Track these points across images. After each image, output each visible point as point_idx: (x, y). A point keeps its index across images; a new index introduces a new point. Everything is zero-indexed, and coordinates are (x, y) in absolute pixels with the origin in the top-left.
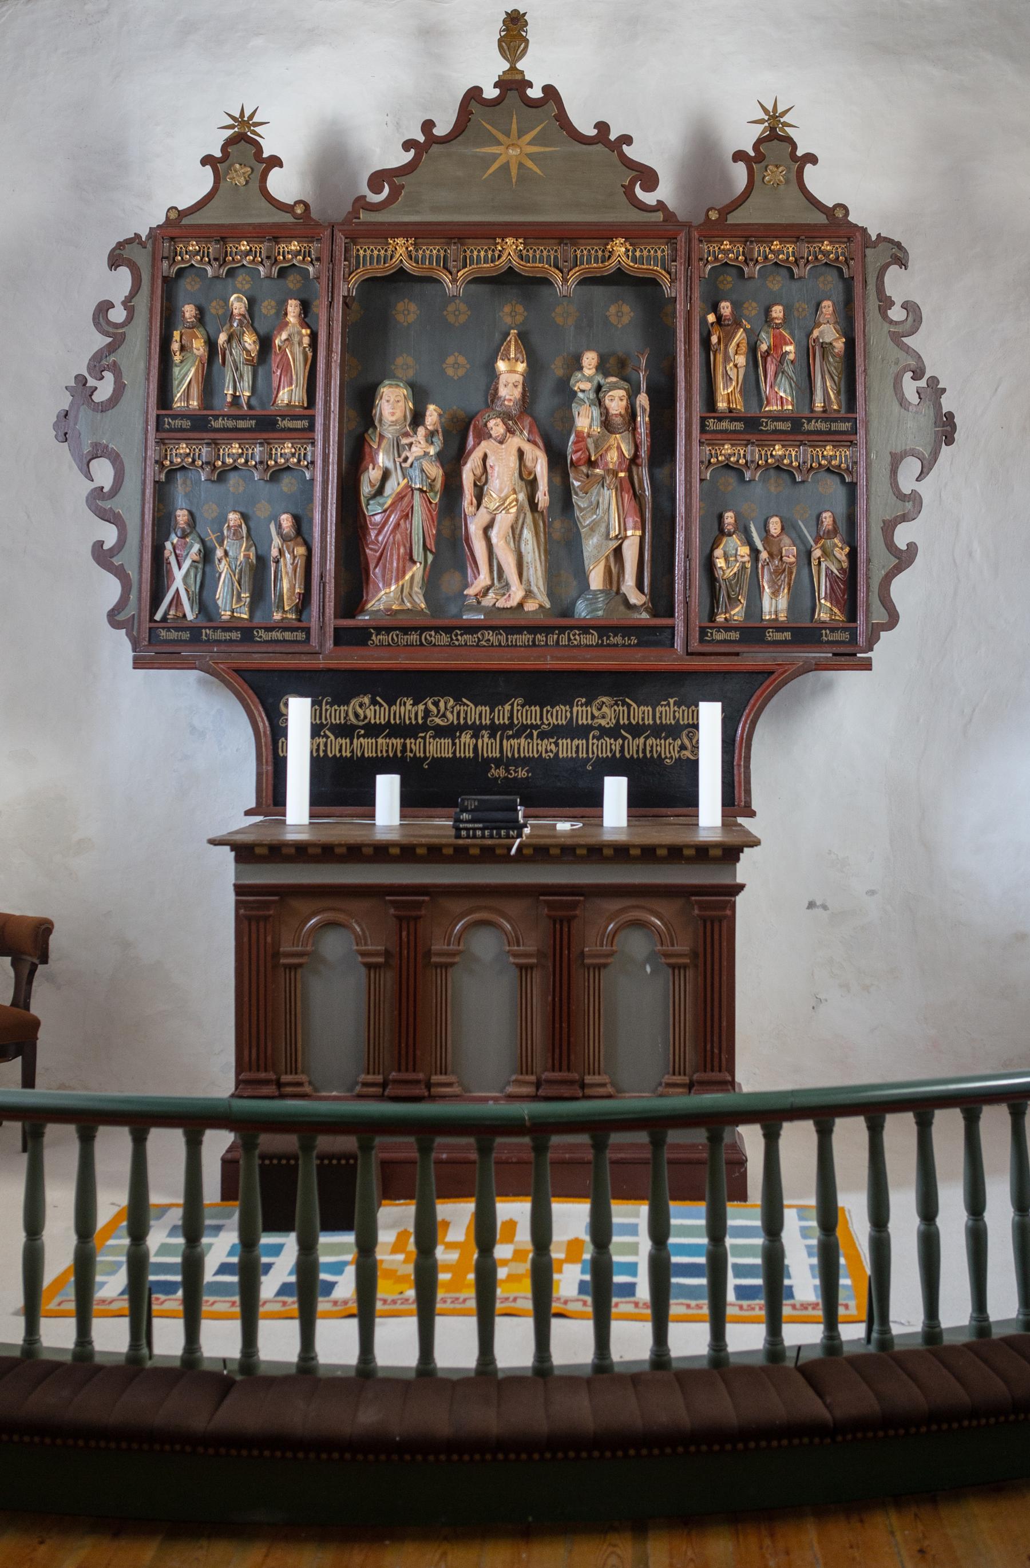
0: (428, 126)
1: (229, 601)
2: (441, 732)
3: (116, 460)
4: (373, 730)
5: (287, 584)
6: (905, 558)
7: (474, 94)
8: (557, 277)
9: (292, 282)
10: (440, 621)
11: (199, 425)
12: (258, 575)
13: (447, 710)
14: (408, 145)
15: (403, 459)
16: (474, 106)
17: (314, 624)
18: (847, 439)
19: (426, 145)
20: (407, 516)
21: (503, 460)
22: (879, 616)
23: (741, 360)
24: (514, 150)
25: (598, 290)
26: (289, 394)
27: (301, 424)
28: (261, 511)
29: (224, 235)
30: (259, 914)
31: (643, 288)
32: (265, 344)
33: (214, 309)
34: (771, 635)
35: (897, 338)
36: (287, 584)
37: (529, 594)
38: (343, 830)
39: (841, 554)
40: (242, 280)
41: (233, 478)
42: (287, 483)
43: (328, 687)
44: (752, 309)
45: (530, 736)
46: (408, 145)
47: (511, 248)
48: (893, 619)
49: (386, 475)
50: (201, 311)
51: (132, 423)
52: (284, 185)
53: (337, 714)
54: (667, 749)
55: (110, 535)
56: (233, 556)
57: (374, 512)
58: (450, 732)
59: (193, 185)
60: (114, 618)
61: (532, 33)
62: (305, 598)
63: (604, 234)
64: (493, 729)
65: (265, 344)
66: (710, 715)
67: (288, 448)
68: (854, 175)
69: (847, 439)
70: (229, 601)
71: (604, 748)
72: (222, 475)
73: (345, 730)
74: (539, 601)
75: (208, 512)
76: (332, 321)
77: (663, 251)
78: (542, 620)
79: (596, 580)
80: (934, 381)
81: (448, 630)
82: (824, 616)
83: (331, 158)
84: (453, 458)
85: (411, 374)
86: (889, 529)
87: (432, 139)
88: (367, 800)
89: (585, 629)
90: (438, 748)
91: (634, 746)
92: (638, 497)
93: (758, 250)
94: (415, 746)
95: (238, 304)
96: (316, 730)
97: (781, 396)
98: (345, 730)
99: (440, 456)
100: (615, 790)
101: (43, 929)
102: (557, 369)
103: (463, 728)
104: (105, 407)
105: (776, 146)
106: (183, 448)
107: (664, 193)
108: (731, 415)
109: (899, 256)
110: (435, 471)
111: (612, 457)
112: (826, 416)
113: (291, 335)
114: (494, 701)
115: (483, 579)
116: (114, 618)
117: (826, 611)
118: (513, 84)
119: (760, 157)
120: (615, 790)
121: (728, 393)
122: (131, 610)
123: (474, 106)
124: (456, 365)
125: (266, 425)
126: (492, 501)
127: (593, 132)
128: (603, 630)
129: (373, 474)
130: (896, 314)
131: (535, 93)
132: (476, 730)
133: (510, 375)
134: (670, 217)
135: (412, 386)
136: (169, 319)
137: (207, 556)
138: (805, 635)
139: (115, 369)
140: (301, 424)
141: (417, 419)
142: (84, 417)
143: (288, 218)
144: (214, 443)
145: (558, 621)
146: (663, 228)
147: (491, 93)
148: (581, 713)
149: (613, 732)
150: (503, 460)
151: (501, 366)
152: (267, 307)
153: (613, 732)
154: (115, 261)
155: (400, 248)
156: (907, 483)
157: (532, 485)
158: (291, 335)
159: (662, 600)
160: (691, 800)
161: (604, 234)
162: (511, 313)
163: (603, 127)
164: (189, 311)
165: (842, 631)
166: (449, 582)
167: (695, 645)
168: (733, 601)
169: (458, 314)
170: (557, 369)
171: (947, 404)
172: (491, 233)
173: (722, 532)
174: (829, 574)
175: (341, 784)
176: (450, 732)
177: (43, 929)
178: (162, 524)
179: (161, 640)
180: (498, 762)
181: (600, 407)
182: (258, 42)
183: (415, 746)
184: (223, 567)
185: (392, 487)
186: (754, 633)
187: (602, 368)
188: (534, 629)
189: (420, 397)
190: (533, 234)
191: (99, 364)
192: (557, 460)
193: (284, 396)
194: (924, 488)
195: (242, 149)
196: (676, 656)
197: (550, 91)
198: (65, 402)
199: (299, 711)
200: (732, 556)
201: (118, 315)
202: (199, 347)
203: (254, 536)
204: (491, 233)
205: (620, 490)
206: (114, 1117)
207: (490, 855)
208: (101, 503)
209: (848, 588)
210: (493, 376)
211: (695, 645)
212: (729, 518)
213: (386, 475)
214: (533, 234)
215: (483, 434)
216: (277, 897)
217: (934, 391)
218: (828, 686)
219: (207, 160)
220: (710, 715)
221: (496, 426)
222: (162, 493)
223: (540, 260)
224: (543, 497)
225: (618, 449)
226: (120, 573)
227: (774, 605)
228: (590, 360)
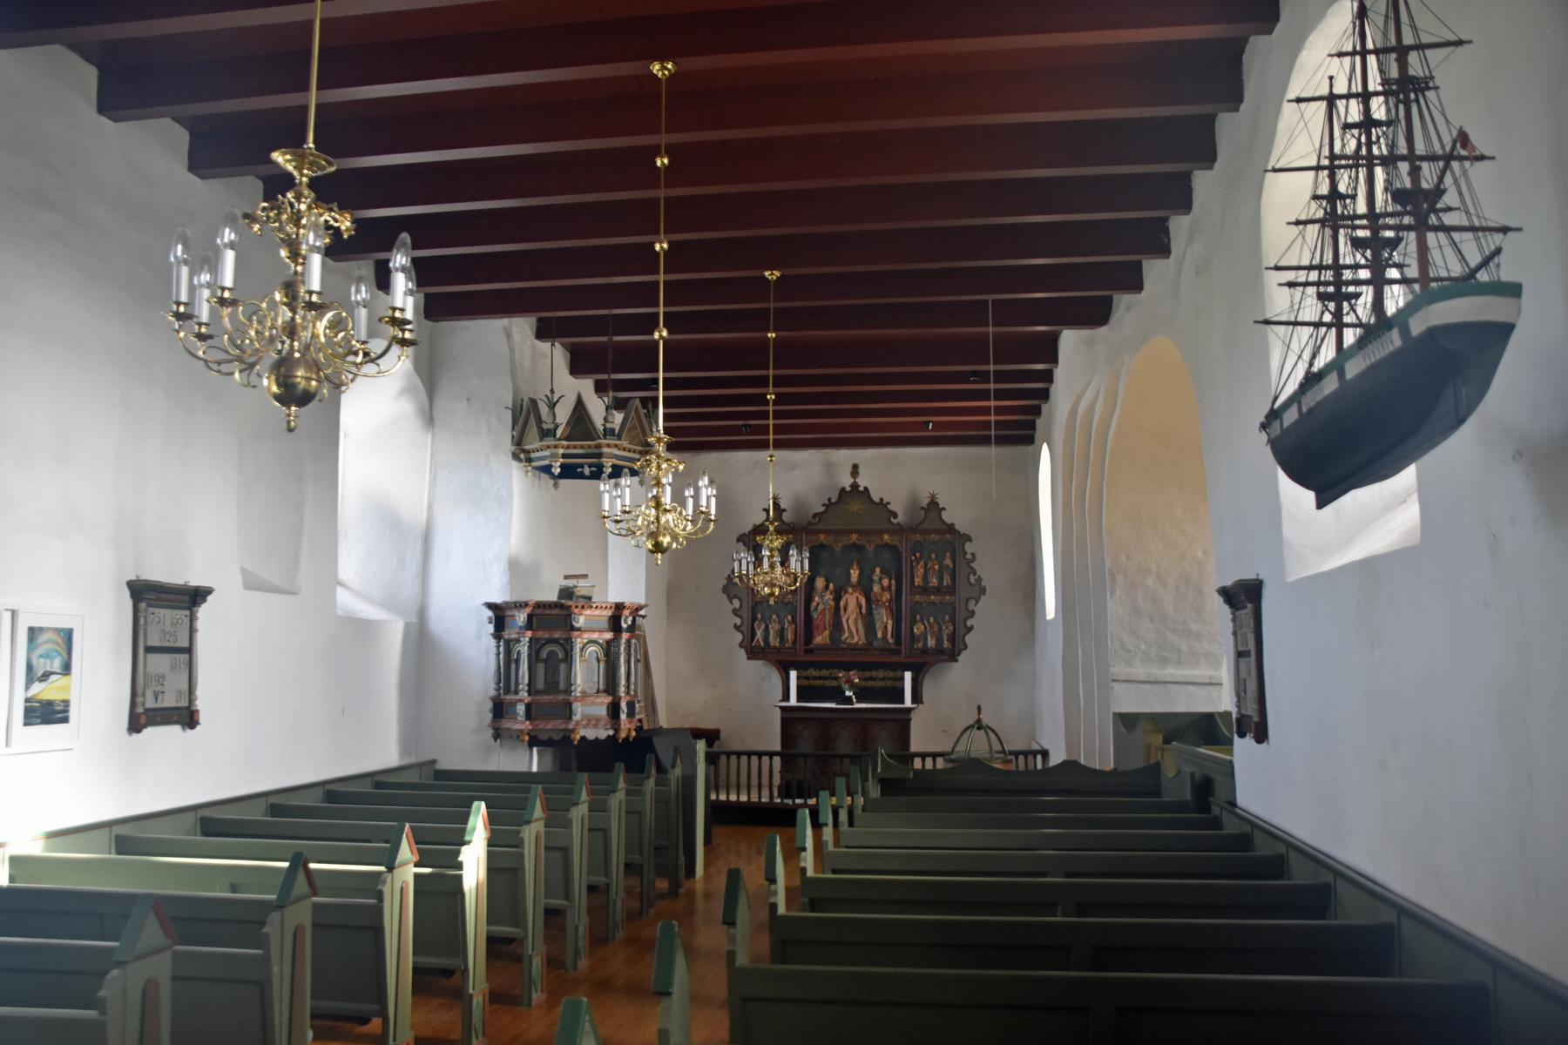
1: (774, 641)
4: (815, 678)
5: (790, 636)
6: (970, 629)
7: (843, 489)
12: (781, 634)
19: (829, 505)
21: (852, 600)
24: (855, 506)
31: (894, 549)
36: (790, 636)
48: (966, 647)
54: (897, 684)
55: (738, 621)
56: (774, 628)
57: (815, 616)
60: (741, 645)
62: (795, 641)
63: (882, 532)
66: (908, 676)
70: (774, 641)
73: (807, 678)
74: (863, 641)
79: (879, 635)
84: (837, 599)
86: (965, 621)
97: (934, 581)
105: (933, 506)
107: (901, 519)
109: (969, 539)
116: (741, 645)
117: (946, 644)
118: (855, 486)
121: (917, 581)
133: (854, 574)
136: (754, 619)
141: (827, 587)
146: (899, 530)
148: (874, 674)
150: (852, 600)
156: (971, 607)
157: (860, 607)
165: (951, 652)
178: (754, 619)
179: (754, 653)
181: (881, 584)
186: (925, 651)
189: (828, 582)
192: (868, 600)
199: (793, 674)
200: (918, 629)
203: (781, 622)
206: (744, 753)
208: (736, 612)
217: (979, 580)
220: (908, 676)
225: (887, 596)
227: (931, 643)
228: (878, 570)
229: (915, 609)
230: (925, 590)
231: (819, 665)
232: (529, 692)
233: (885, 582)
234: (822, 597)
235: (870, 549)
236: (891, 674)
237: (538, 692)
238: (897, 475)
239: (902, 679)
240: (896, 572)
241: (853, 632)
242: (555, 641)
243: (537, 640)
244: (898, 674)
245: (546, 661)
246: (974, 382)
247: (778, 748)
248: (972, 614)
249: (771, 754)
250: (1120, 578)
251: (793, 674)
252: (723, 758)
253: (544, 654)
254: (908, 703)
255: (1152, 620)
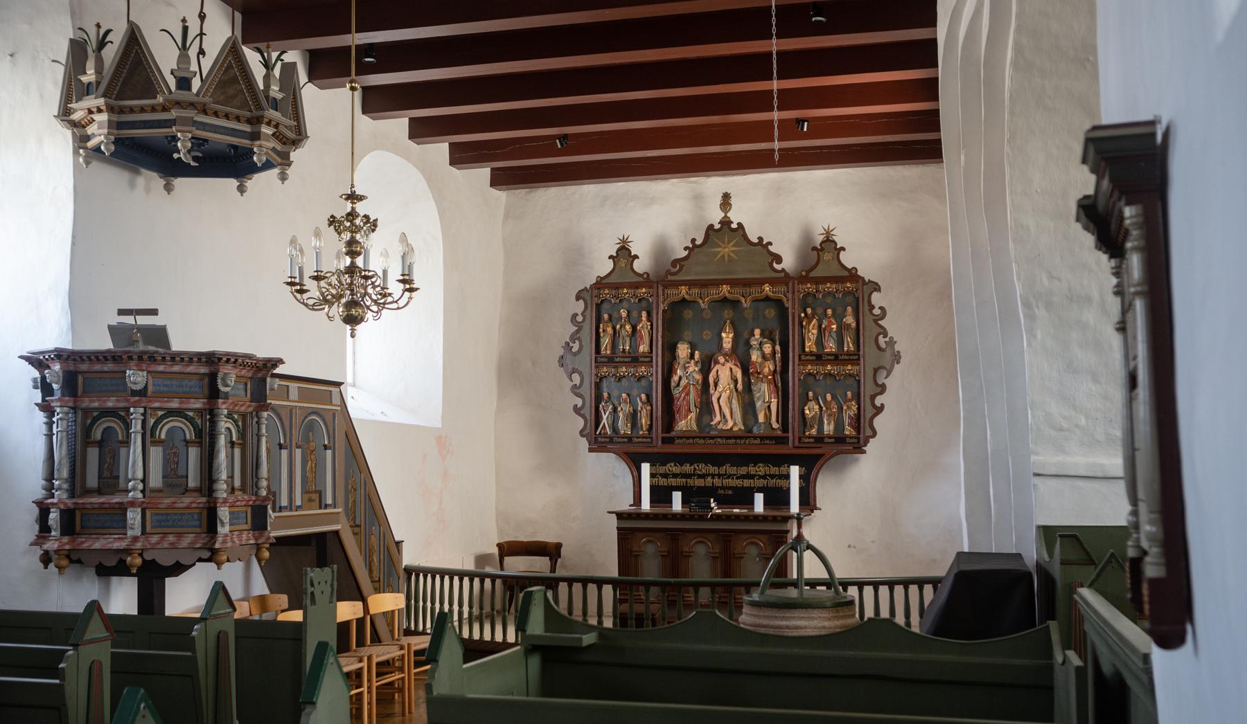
0: (693, 241)
1: (624, 427)
2: (700, 476)
3: (580, 374)
4: (675, 476)
5: (644, 421)
6: (880, 410)
7: (711, 227)
8: (743, 300)
9: (644, 304)
10: (704, 431)
11: (610, 360)
12: (633, 417)
13: (702, 468)
14: (686, 248)
15: (687, 373)
16: (711, 232)
17: (654, 436)
18: (856, 362)
19: (693, 248)
20: (688, 394)
21: (725, 373)
22: (869, 432)
23: (815, 332)
24: (726, 249)
25: (761, 304)
26: (643, 348)
27: (648, 359)
28: (635, 392)
29: (617, 286)
30: (625, 536)
32: (634, 328)
33: (615, 315)
34: (826, 440)
35: (876, 321)
36: (644, 421)
37: (735, 424)
38: (660, 510)
39: (855, 408)
40: (625, 304)
41: (624, 380)
42: (643, 382)
43: (653, 459)
44: (820, 311)
45: (732, 477)
46: (686, 248)
47: (725, 289)
48: (874, 434)
49: (680, 378)
50: (610, 316)
51: (586, 360)
52: (640, 266)
53: (662, 470)
54: (781, 483)
55: (579, 402)
57: (676, 392)
58: (703, 476)
59: (606, 267)
61: (733, 201)
62: (651, 426)
63: (761, 282)
64: (719, 476)
65: (634, 328)
66: (795, 471)
67: (643, 369)
68: (862, 254)
69: (856, 362)
70: (624, 427)
71: (760, 483)
72: (620, 379)
73: (665, 476)
75: (615, 393)
76: (659, 319)
77: (783, 289)
78: (740, 434)
79: (761, 419)
80: (891, 338)
81: (704, 438)
82: (847, 433)
83: (661, 250)
84: (705, 370)
85: (690, 339)
86: (873, 398)
87: (695, 246)
88: (669, 501)
89: (755, 438)
90: (699, 482)
91: (772, 483)
92: (776, 386)
93: (821, 287)
94: (690, 482)
95: (624, 313)
96: (652, 476)
97: (831, 346)
98: (665, 476)
99: (701, 370)
100: (759, 499)
101: (558, 546)
102: (746, 335)
103: (708, 475)
104: (575, 354)
105: (829, 245)
106: (605, 369)
108: (811, 354)
109: (877, 288)
110: (699, 377)
111: (766, 370)
112: (848, 354)
113: (644, 327)
114: (720, 465)
115: (718, 418)
116: (582, 433)
117: (848, 431)
118: (726, 222)
119: (822, 249)
120: (759, 499)
121: (810, 346)
122: (587, 431)
123: (711, 232)
124: (707, 335)
125: (635, 360)
126: (720, 388)
127: (756, 241)
128: (762, 438)
129: (676, 378)
130: (877, 311)
131: (734, 226)
132: (713, 476)
133: (727, 338)
134: (787, 274)
135: (690, 343)
136: (599, 319)
137: (615, 409)
138: (840, 439)
139: (579, 339)
140: (648, 359)
141: (692, 356)
142: (569, 358)
143: (641, 279)
144: (616, 367)
145: (747, 434)
146: (784, 279)
147: (717, 226)
148: (752, 470)
149: (764, 477)
150: (725, 373)
151: (724, 335)
152: (635, 314)
153: (764, 477)
154: (578, 298)
155: (684, 290)
157: (736, 382)
158: (644, 327)
159: (785, 427)
160: (787, 503)
161: (761, 282)
162: (728, 313)
163: (760, 239)
164: (606, 316)
165: (852, 442)
166: (705, 419)
167: (797, 444)
168: (812, 427)
169: (708, 315)
170: (746, 335)
171: (1114, 281)
172: (717, 283)
173: (808, 400)
174: (850, 417)
175: (660, 495)
176: (703, 476)
177: (558, 546)
178: (598, 399)
179: (599, 443)
180: (721, 488)
181: (761, 351)
182: (631, 204)
183: (690, 482)
184: (621, 414)
185: (683, 383)
186: (820, 439)
187: (762, 335)
188: (736, 438)
189: (693, 347)
190: (733, 283)
191: (574, 338)
192: (745, 372)
193: (641, 349)
194: (887, 382)
195: (624, 253)
196: (788, 449)
197: (740, 225)
198: (561, 352)
199: (646, 468)
200: (811, 410)
201: (580, 318)
202: (610, 330)
203: (632, 403)
204: (717, 283)
205: (769, 383)
207: (702, 518)
208: (575, 390)
209: (857, 421)
210: (721, 339)
211: (797, 444)
212: (811, 394)
213: (680, 378)
214: (733, 283)
215: (717, 362)
216: (631, 528)
217: (891, 343)
218: (857, 460)
219: (611, 257)
220: (795, 471)
221: (721, 359)
222: (598, 386)
223: (736, 293)
224: (740, 387)
225: (769, 367)
226: (583, 416)
227: (828, 428)
228: (757, 332)
229: (808, 381)
230: (819, 358)
231: (681, 459)
232: (72, 493)
233: (767, 348)
234: (685, 368)
235: (746, 303)
236: (774, 470)
237: (87, 492)
238: (787, 206)
239: (787, 477)
240: (782, 337)
241: (727, 415)
242: (178, 413)
243: (87, 412)
244: (783, 470)
245: (100, 444)
246: (819, 30)
247: (614, 572)
248: (883, 389)
249: (600, 582)
250: (1041, 312)
251: (646, 468)
252: (563, 587)
253: (97, 434)
254: (795, 508)
255: (1095, 380)
